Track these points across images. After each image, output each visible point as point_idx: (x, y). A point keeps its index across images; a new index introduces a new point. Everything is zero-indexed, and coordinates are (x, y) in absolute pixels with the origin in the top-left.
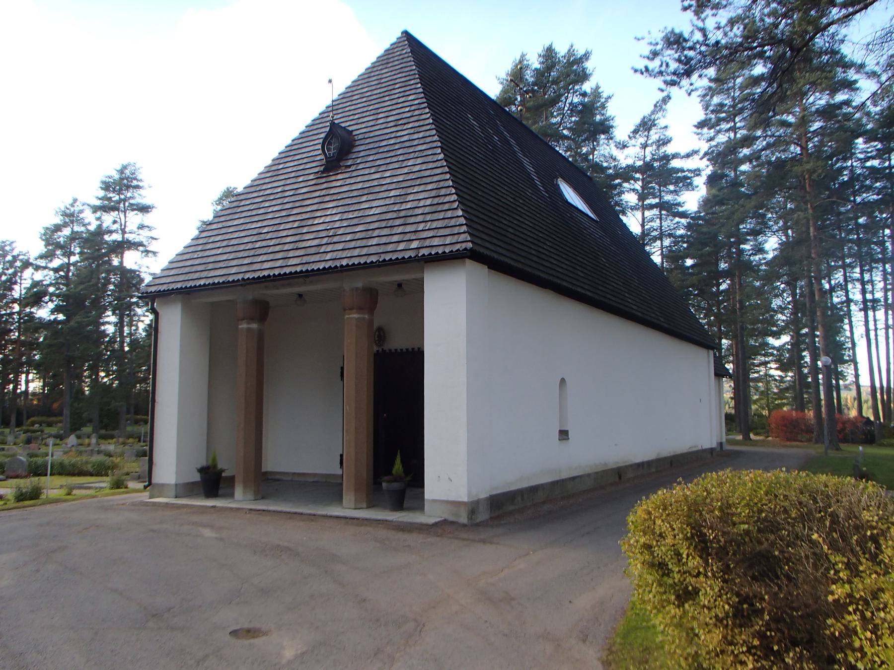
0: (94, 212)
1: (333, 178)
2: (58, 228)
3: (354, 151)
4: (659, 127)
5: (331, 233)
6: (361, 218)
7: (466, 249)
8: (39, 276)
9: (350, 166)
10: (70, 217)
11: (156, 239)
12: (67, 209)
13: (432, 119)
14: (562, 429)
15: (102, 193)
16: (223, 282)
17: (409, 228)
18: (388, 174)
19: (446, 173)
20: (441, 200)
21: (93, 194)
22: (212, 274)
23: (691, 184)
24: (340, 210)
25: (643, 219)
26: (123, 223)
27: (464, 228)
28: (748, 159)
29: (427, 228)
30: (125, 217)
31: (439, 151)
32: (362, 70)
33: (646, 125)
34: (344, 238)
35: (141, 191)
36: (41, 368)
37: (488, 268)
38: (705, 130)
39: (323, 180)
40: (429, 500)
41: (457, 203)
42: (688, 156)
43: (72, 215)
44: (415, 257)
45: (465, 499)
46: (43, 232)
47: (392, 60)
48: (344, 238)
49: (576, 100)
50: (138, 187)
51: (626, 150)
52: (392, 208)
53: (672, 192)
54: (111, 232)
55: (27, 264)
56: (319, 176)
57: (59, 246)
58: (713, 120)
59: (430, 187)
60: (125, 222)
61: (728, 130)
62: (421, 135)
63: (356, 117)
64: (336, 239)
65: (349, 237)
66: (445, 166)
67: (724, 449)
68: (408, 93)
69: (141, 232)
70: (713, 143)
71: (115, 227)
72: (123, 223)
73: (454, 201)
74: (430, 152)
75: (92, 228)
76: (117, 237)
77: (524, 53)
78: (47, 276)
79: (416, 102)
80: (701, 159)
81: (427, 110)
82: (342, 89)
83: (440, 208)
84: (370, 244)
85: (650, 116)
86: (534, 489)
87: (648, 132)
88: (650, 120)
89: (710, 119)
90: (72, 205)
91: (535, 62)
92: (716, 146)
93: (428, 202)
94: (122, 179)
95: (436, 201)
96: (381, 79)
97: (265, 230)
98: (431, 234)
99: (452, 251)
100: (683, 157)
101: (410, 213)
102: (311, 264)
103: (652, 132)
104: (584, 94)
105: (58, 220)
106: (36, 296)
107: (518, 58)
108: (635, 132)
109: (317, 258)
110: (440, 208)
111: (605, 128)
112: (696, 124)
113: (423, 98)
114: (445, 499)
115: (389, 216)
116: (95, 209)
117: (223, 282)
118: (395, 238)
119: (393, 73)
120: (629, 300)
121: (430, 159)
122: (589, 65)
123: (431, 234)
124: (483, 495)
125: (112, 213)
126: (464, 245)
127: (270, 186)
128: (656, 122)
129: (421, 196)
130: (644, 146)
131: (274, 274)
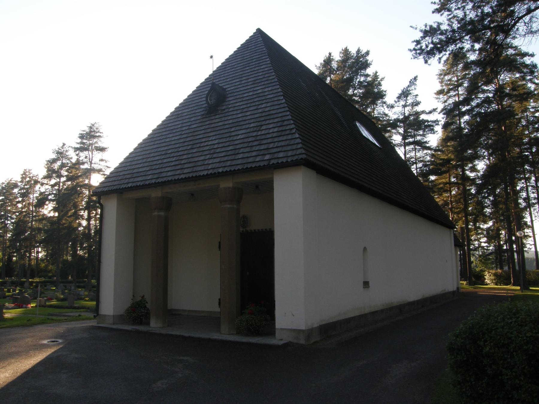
0: (75, 151)
1: (213, 118)
2: (54, 161)
3: (227, 100)
4: (413, 95)
5: (212, 151)
6: (232, 142)
7: (302, 159)
8: (43, 190)
9: (224, 110)
10: (61, 154)
11: (109, 167)
12: (60, 150)
13: (277, 79)
14: (365, 281)
15: (79, 140)
16: (143, 185)
17: (263, 147)
18: (248, 113)
19: (287, 111)
20: (284, 128)
21: (74, 141)
22: (136, 180)
23: (433, 130)
24: (217, 137)
25: (405, 151)
26: (91, 158)
27: (300, 146)
28: (468, 112)
29: (275, 146)
30: (92, 154)
31: (282, 98)
32: (232, 52)
33: (405, 94)
34: (220, 155)
35: (101, 139)
36: (45, 243)
37: (317, 173)
38: (441, 96)
39: (207, 119)
40: (278, 329)
41: (295, 130)
42: (430, 112)
43: (61, 153)
44: (267, 165)
45: (303, 328)
46: (46, 163)
47: (250, 46)
48: (220, 155)
49: (362, 79)
50: (99, 136)
51: (394, 110)
52: (251, 134)
53: (421, 135)
54: (83, 163)
55: (36, 182)
56: (204, 117)
57: (54, 171)
58: (446, 90)
59: (276, 120)
60: (92, 157)
61: (455, 96)
62: (270, 89)
63: (228, 80)
64: (215, 155)
65: (223, 154)
66: (286, 107)
67: (460, 291)
68: (261, 64)
69: (101, 163)
70: (446, 104)
71: (85, 160)
72: (91, 158)
73: (293, 128)
74: (276, 99)
75: (74, 160)
76: (86, 166)
77: (331, 52)
78: (48, 189)
79: (266, 69)
80: (439, 113)
81: (274, 74)
82: (219, 64)
83: (283, 133)
84: (237, 158)
85: (407, 88)
86: (348, 321)
87: (407, 98)
88: (407, 90)
89: (444, 90)
90: (62, 147)
91: (337, 57)
92: (448, 105)
93: (276, 130)
94: (91, 132)
95: (281, 129)
96: (244, 57)
97: (170, 151)
98: (278, 150)
99: (292, 161)
100: (427, 113)
101: (263, 137)
102: (199, 172)
103: (408, 98)
104: (367, 76)
105: (54, 156)
106: (42, 201)
107: (328, 55)
108: (399, 98)
109: (202, 168)
110: (283, 133)
111: (381, 95)
112: (436, 92)
113: (270, 67)
114: (290, 328)
115: (250, 139)
116: (76, 149)
117: (143, 185)
118: (254, 154)
119: (252, 53)
120: (404, 197)
121: (276, 103)
122: (369, 58)
123: (278, 150)
124: (316, 325)
125: (85, 152)
126: (301, 157)
127: (173, 124)
128: (410, 92)
129: (271, 126)
130: (404, 106)
131: (175, 179)
